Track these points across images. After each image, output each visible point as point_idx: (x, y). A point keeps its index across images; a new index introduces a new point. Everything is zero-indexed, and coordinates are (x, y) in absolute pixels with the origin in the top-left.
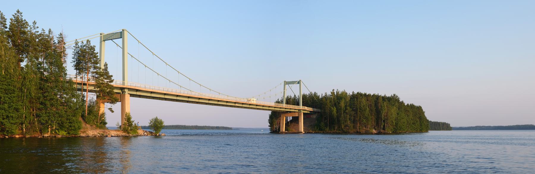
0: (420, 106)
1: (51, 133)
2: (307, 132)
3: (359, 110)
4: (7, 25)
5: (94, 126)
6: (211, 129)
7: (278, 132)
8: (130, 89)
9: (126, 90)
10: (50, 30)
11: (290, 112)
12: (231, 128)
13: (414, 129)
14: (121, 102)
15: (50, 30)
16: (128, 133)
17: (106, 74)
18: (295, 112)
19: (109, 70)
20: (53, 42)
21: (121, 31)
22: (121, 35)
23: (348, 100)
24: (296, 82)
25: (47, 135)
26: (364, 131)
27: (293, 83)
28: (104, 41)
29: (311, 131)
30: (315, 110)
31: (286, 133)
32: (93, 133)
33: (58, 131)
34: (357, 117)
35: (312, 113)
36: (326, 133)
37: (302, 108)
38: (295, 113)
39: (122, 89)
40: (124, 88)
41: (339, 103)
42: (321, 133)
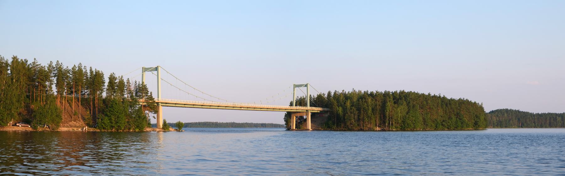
3: (362, 110)
6: (253, 127)
8: (162, 103)
9: (160, 104)
10: (122, 76)
11: (299, 112)
15: (122, 76)
16: (165, 130)
17: (151, 98)
19: (153, 96)
22: (156, 69)
23: (355, 100)
27: (301, 86)
28: (296, 87)
29: (320, 129)
30: (326, 109)
31: (296, 130)
39: (157, 103)
41: (345, 103)
42: (329, 130)
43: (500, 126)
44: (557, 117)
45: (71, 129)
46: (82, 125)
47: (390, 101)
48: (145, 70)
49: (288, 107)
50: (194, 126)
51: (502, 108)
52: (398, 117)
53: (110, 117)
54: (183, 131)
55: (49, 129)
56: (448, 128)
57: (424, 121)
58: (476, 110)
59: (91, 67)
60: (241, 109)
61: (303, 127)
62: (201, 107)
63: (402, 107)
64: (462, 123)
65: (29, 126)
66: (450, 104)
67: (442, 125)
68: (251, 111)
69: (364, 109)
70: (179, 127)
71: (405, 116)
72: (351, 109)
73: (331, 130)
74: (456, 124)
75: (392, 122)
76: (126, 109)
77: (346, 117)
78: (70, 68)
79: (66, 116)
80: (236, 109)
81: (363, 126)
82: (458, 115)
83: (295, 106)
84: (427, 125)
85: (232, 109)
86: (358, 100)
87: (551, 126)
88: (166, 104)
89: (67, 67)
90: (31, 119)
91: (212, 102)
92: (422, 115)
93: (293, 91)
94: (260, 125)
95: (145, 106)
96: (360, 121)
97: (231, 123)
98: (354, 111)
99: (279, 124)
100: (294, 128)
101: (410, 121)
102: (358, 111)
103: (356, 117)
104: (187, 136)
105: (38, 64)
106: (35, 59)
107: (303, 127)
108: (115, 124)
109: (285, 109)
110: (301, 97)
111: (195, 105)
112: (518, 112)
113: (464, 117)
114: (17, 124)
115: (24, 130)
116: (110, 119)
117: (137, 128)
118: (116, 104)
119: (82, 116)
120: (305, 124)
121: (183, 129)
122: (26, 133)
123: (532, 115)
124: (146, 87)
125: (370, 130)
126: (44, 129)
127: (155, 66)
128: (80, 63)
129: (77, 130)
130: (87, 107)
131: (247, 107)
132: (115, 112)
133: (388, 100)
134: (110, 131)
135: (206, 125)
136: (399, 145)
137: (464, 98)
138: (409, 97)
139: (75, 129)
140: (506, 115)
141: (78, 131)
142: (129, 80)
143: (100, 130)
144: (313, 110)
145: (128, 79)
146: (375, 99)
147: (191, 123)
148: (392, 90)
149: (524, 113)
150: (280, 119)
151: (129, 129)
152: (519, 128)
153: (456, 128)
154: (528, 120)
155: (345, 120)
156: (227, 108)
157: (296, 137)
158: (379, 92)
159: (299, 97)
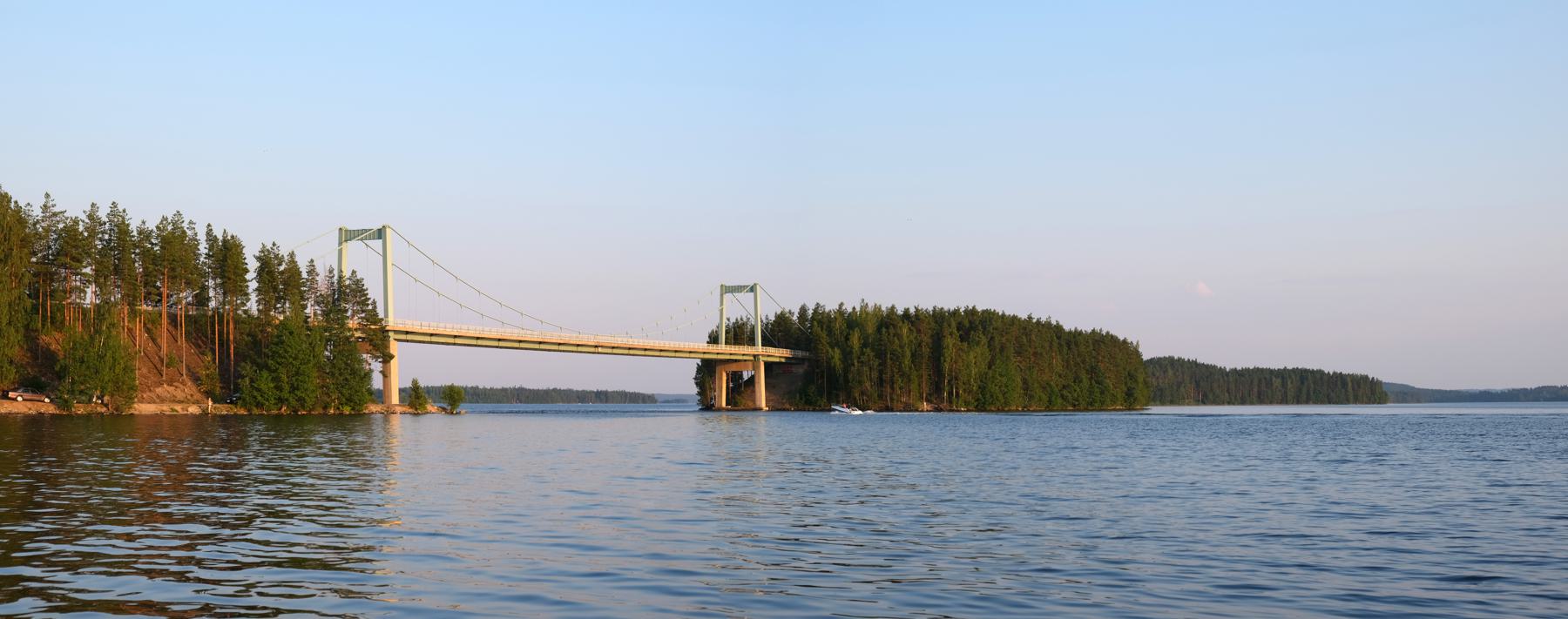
0: (1108, 333)
2: (775, 408)
3: (888, 356)
4: (195, 224)
6: (576, 402)
8: (396, 332)
9: (391, 334)
11: (736, 361)
12: (653, 395)
16: (416, 409)
22: (380, 234)
23: (871, 329)
24: (747, 286)
27: (739, 289)
28: (346, 241)
29: (788, 406)
30: (800, 354)
31: (728, 410)
34: (886, 373)
35: (793, 361)
37: (760, 350)
38: (747, 363)
41: (847, 339)
43: (1160, 401)
44: (1274, 379)
45: (166, 408)
46: (192, 395)
47: (951, 334)
48: (347, 235)
49: (702, 345)
51: (1162, 356)
52: (970, 375)
53: (275, 371)
54: (463, 411)
55: (105, 409)
56: (1074, 406)
57: (1026, 386)
58: (1129, 360)
59: (209, 225)
60: (596, 350)
61: (744, 401)
62: (496, 344)
63: (978, 350)
64: (1102, 393)
65: (47, 400)
66: (1076, 345)
67: (1062, 396)
68: (576, 354)
69: (894, 355)
70: (452, 399)
71: (986, 374)
72: (863, 354)
73: (814, 410)
74: (1090, 394)
75: (957, 388)
76: (316, 350)
77: (850, 376)
78: (151, 225)
79: (144, 371)
80: (585, 352)
81: (892, 399)
82: (1093, 371)
83: (724, 345)
84: (1031, 397)
86: (879, 329)
87: (1262, 399)
88: (407, 335)
89: (144, 223)
90: (43, 379)
92: (1021, 370)
93: (719, 304)
94: (594, 395)
95: (363, 339)
96: (884, 385)
97: (514, 389)
98: (869, 361)
99: (642, 394)
100: (724, 404)
101: (996, 385)
102: (879, 358)
103: (875, 375)
104: (471, 425)
105: (56, 210)
106: (47, 196)
107: (744, 401)
108: (290, 392)
109: (690, 352)
110: (737, 320)
111: (436, 335)
112: (1194, 366)
113: (1105, 378)
114: (11, 394)
115: (33, 412)
116: (276, 379)
117: (346, 404)
118: (291, 333)
119: (188, 367)
120: (749, 392)
121: (463, 407)
122: (35, 421)
123: (1222, 371)
124: (363, 285)
125: (908, 408)
126: (90, 409)
127: (376, 226)
128: (178, 212)
129: (182, 409)
130: (200, 342)
131: (613, 345)
132: (291, 356)
133: (946, 332)
134: (275, 412)
137: (1101, 330)
138: (991, 324)
139: (178, 407)
140: (1170, 372)
141: (186, 412)
142: (315, 263)
143: (249, 411)
144: (769, 356)
145: (312, 261)
146: (916, 328)
148: (949, 305)
149: (1207, 367)
150: (681, 379)
151: (325, 408)
152: (1198, 405)
153: (1091, 404)
154: (1215, 385)
155: (848, 382)
156: (562, 348)
157: (722, 426)
158: (922, 310)
159: (733, 320)
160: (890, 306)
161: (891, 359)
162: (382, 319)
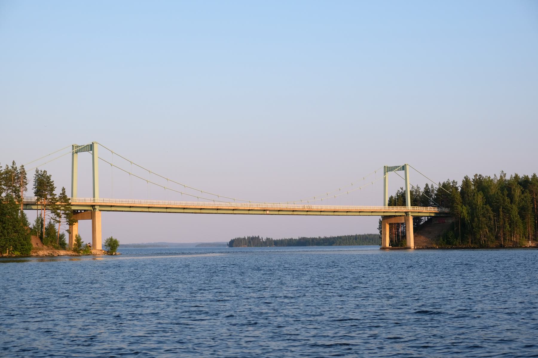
1: (9, 253)
5: (51, 247)
7: (504, 246)
9: (410, 213)
10: (14, 161)
11: (394, 216)
13: (27, 249)
14: (91, 220)
15: (14, 161)
18: (401, 216)
20: (17, 172)
21: (91, 144)
22: (404, 168)
25: (5, 255)
26: (511, 244)
28: (387, 172)
29: (435, 246)
32: (43, 253)
33: (14, 252)
36: (482, 247)
39: (93, 206)
40: (95, 205)
50: (346, 243)
62: (232, 212)
80: (104, 211)
81: (505, 239)
85: (216, 213)
91: (213, 203)
100: (387, 245)
106: (495, 175)
125: (516, 246)
135: (367, 241)
136: (328, 284)
145: (23, 166)
146: (529, 190)
147: (340, 238)
156: (151, 210)
160: (533, 175)
161: (503, 212)
162: (69, 199)
